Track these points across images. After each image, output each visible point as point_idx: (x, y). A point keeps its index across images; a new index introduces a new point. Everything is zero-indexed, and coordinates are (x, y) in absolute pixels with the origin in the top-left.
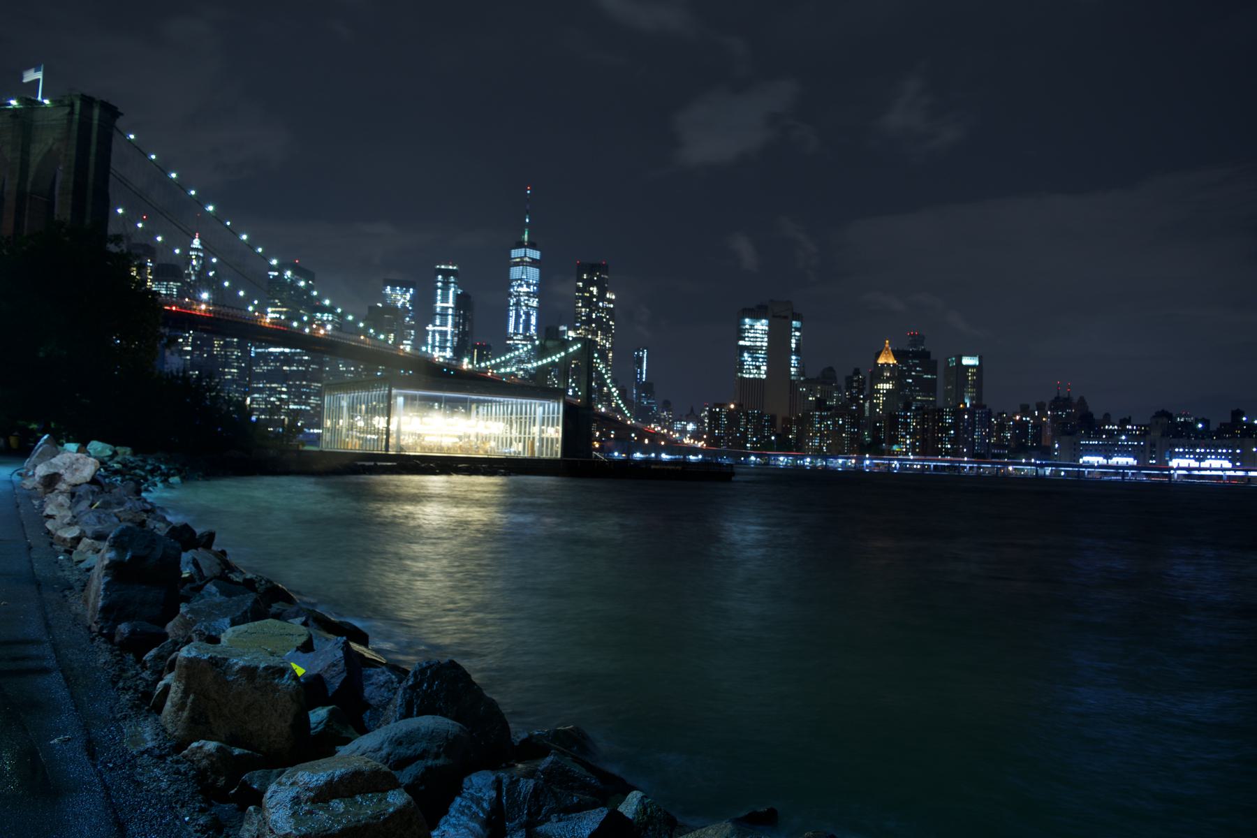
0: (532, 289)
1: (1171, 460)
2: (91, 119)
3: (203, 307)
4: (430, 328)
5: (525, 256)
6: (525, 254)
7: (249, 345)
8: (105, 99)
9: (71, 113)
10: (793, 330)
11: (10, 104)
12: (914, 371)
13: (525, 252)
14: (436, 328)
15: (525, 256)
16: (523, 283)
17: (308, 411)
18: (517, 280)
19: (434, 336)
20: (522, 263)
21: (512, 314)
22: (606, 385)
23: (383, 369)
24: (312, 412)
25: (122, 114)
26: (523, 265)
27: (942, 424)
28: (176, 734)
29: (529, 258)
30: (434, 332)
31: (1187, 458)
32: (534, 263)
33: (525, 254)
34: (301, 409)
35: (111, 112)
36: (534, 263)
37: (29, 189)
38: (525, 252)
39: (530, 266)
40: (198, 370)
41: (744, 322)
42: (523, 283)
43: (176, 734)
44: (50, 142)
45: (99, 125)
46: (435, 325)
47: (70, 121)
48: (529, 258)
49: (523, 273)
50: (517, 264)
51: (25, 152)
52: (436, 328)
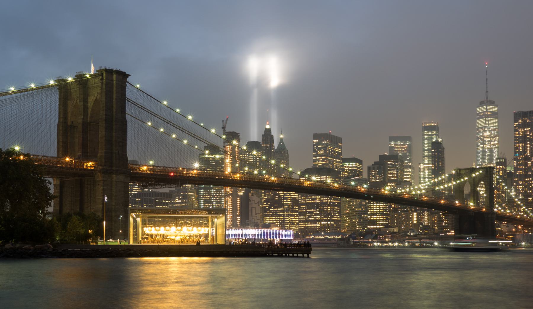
0: (227, 165)
2: (113, 81)
3: (195, 171)
4: (422, 166)
5: (487, 111)
6: (487, 109)
8: (118, 69)
9: (102, 79)
12: (367, 202)
13: (487, 108)
14: (426, 166)
15: (487, 111)
16: (486, 129)
17: (333, 224)
19: (424, 171)
20: (485, 116)
22: (521, 200)
24: (335, 225)
25: (130, 75)
26: (486, 117)
29: (490, 112)
30: (424, 168)
31: (291, 257)
32: (494, 115)
33: (487, 109)
34: (316, 226)
35: (123, 76)
36: (494, 115)
37: (89, 121)
38: (487, 108)
39: (490, 117)
40: (121, 215)
41: (305, 176)
42: (486, 129)
44: (96, 95)
45: (116, 83)
46: (425, 164)
47: (102, 83)
48: (490, 112)
50: (481, 117)
51: (85, 100)
52: (426, 166)
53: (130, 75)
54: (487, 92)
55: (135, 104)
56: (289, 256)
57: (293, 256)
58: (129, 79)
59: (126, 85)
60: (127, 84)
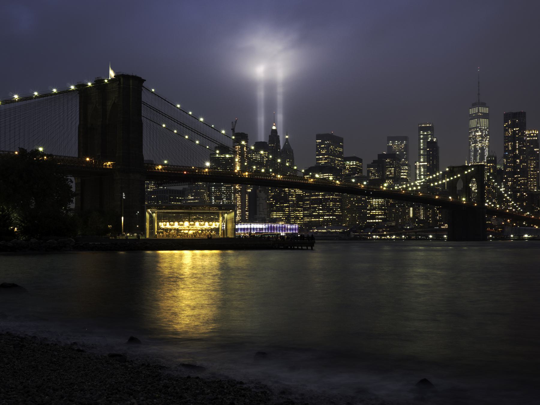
1: (73, 192)
4: (418, 164)
5: (479, 112)
6: (478, 111)
7: (495, 216)
10: (523, 156)
11: (88, 85)
13: (478, 110)
15: (479, 112)
18: (474, 128)
20: (477, 116)
21: (327, 174)
23: (322, 194)
25: (145, 80)
27: (497, 185)
28: (234, 303)
29: (481, 113)
30: (420, 166)
32: (485, 116)
33: (478, 111)
36: (485, 116)
38: (478, 110)
43: (234, 303)
46: (420, 162)
48: (481, 113)
49: (477, 123)
53: (145, 80)
54: (479, 94)
55: (150, 107)
56: (294, 249)
57: (298, 249)
58: (144, 84)
59: (142, 89)
60: (143, 88)
